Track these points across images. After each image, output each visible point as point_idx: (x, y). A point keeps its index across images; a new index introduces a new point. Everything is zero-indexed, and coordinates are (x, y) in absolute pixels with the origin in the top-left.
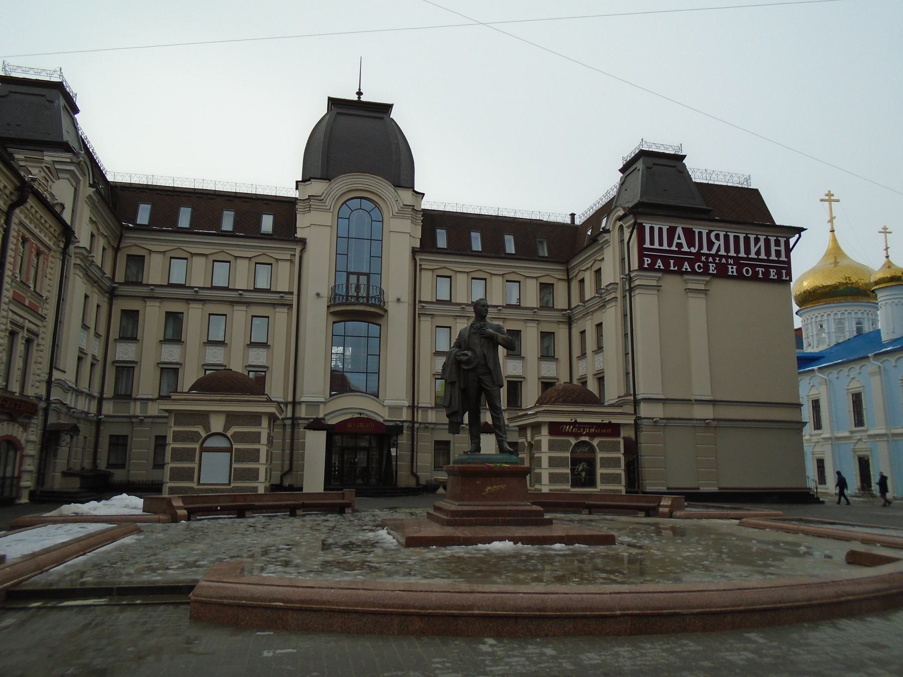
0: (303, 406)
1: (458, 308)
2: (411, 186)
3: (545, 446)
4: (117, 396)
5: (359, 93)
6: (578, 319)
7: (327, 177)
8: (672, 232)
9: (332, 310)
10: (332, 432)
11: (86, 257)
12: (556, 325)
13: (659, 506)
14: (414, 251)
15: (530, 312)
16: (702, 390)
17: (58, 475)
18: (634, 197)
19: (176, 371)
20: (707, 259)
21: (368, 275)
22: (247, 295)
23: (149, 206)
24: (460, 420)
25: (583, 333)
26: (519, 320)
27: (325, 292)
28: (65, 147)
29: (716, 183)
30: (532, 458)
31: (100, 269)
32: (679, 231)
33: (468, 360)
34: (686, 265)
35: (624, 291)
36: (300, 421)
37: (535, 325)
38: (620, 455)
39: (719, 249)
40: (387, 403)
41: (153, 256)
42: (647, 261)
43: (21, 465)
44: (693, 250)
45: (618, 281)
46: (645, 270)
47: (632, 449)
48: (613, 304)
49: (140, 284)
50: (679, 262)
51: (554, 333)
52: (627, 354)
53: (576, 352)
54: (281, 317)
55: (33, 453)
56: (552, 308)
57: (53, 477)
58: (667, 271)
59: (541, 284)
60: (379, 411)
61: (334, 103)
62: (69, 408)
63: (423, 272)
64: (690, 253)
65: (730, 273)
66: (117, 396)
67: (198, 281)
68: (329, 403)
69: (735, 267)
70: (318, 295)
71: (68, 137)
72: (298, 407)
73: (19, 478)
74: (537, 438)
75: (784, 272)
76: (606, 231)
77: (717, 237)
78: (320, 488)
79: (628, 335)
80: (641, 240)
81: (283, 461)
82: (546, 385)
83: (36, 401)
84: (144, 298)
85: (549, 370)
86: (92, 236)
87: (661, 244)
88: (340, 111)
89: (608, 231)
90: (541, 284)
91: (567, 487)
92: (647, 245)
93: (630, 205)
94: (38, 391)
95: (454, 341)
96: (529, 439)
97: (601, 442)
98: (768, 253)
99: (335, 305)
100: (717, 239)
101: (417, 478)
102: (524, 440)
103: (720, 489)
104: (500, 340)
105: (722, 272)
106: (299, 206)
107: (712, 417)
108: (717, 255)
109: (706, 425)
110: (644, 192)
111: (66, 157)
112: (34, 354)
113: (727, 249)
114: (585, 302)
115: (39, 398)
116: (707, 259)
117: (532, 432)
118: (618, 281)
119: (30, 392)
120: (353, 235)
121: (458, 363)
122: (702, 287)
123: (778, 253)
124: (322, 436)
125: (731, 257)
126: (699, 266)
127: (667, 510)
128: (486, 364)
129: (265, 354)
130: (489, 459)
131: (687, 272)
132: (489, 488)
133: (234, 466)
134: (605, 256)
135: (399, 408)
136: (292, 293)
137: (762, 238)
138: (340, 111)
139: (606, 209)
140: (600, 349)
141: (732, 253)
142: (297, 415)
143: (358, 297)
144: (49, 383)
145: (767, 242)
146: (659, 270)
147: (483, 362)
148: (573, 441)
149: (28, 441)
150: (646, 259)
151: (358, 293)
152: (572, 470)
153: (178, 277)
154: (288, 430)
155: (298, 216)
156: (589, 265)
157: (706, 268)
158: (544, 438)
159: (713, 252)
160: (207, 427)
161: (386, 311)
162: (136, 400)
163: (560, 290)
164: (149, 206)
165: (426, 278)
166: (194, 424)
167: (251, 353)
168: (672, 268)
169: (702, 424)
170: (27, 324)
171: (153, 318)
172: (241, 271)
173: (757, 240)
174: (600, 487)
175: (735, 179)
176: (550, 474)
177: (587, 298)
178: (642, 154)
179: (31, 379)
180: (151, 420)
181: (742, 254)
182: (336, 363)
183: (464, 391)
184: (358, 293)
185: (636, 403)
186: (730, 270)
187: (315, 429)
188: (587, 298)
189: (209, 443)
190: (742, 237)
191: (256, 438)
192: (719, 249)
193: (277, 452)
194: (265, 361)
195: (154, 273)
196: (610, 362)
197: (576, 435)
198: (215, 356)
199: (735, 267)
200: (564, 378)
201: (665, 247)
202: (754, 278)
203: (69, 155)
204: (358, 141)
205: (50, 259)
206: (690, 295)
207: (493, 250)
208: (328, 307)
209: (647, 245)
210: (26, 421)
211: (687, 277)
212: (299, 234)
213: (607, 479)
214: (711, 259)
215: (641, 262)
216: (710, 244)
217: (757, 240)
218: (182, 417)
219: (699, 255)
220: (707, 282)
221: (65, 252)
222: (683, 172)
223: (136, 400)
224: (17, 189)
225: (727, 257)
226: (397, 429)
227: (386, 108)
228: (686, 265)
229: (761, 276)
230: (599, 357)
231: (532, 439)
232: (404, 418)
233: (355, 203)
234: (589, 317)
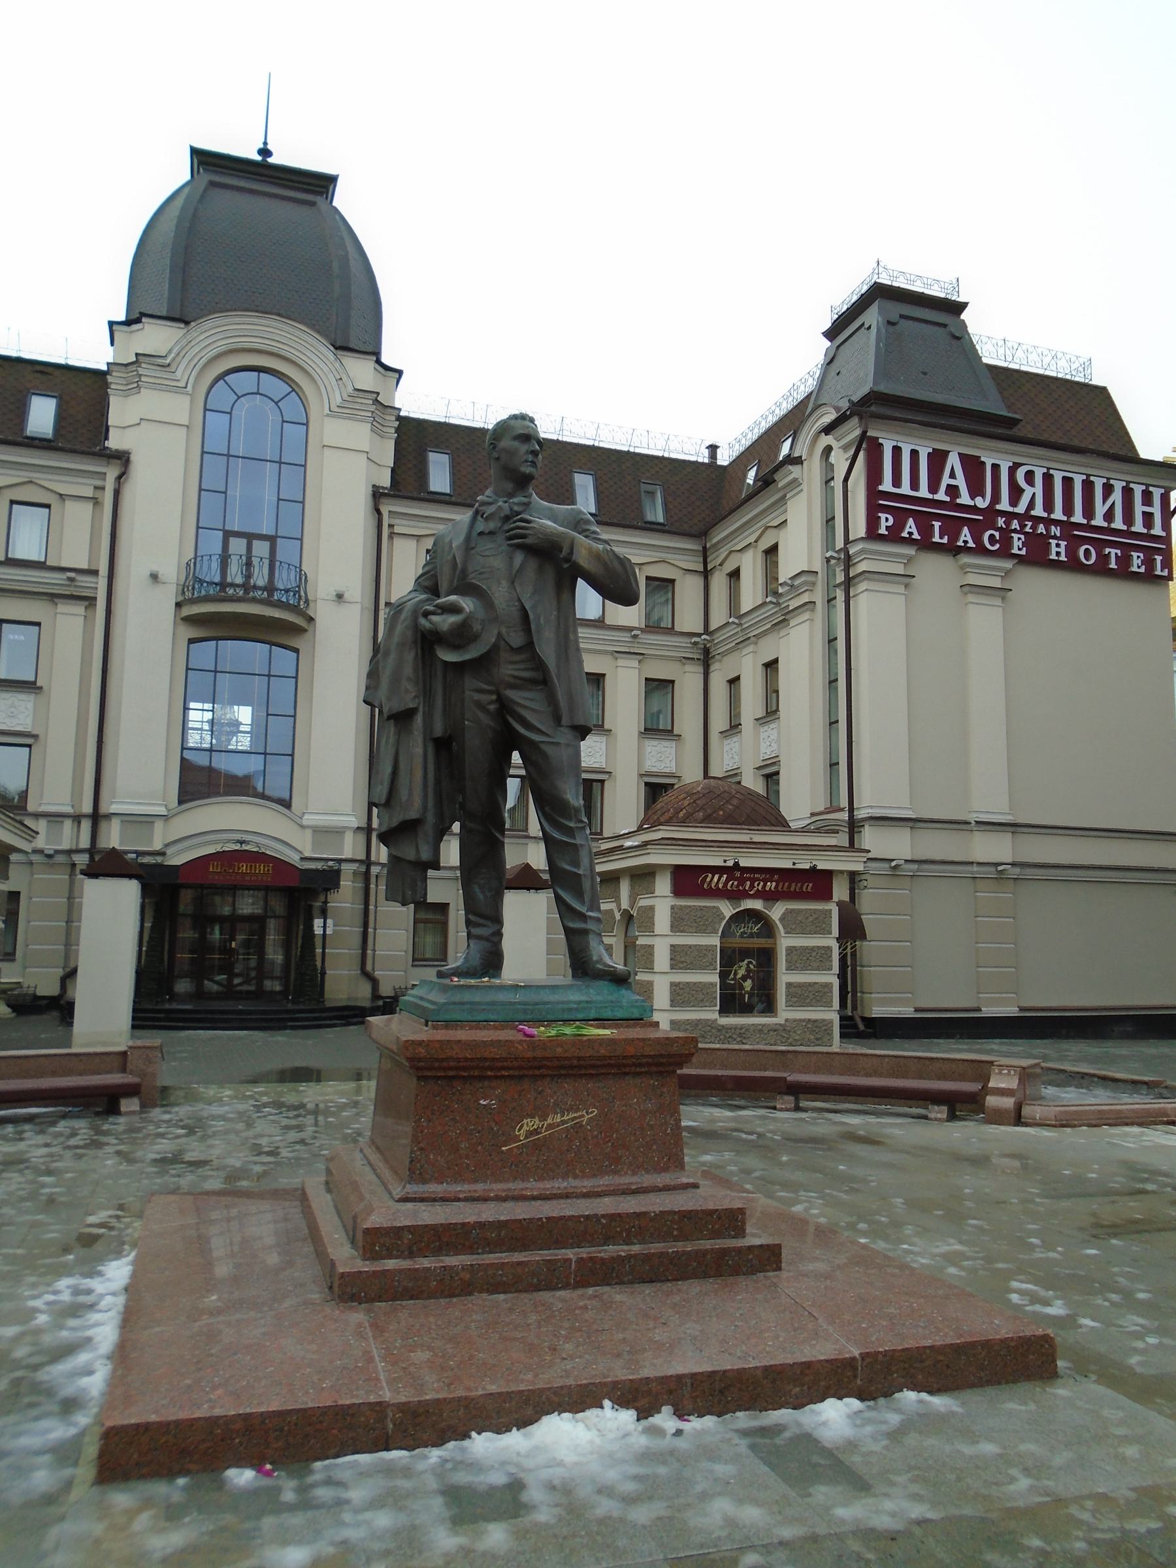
0: (115, 824)
2: (376, 354)
3: (662, 920)
7: (180, 316)
8: (938, 459)
9: (187, 611)
12: (677, 665)
13: (986, 1091)
14: (377, 495)
15: (625, 637)
16: (991, 803)
18: (862, 378)
21: (272, 539)
24: (425, 855)
25: (734, 681)
26: (606, 652)
27: (172, 572)
29: (1024, 368)
30: (630, 946)
32: (953, 461)
33: (464, 626)
34: (965, 535)
35: (830, 586)
37: (635, 664)
38: (831, 942)
40: (308, 819)
42: (886, 521)
44: (981, 503)
45: (818, 566)
46: (881, 538)
47: (852, 929)
48: (806, 616)
50: (952, 527)
51: (673, 682)
52: (833, 723)
53: (719, 721)
54: (68, 628)
56: (670, 631)
58: (925, 544)
60: (289, 838)
61: (205, 160)
63: (397, 542)
64: (974, 509)
65: (1053, 556)
69: (1063, 543)
70: (154, 577)
72: (103, 826)
74: (643, 902)
75: (1159, 558)
76: (792, 460)
79: (839, 683)
82: (655, 790)
85: (661, 758)
87: (915, 485)
88: (217, 178)
89: (798, 461)
92: (887, 486)
93: (855, 399)
96: (625, 904)
98: (1128, 518)
99: (193, 601)
100: (1028, 480)
101: (374, 982)
102: (613, 906)
103: (1022, 1009)
104: (582, 558)
105: (1037, 556)
107: (1010, 860)
108: (1027, 516)
109: (998, 873)
110: (882, 370)
113: (1049, 506)
114: (740, 617)
117: (632, 887)
120: (239, 449)
121: (427, 642)
122: (996, 582)
123: (1148, 518)
124: (128, 892)
125: (1057, 522)
126: (992, 537)
127: (1008, 1103)
128: (529, 646)
129: (30, 705)
130: (533, 1008)
131: (966, 549)
132: (529, 1124)
134: (790, 516)
135: (337, 832)
137: (1118, 486)
138: (217, 178)
139: (792, 422)
140: (771, 713)
141: (1058, 514)
143: (246, 586)
145: (1128, 492)
146: (909, 541)
147: (517, 640)
148: (727, 909)
150: (883, 516)
151: (248, 576)
152: (723, 975)
155: (113, 400)
156: (752, 539)
157: (1006, 541)
158: (662, 900)
161: (311, 620)
163: (688, 591)
173: (1108, 489)
175: (1062, 363)
176: (672, 984)
177: (744, 609)
178: (879, 293)
181: (1078, 517)
183: (444, 747)
185: (854, 826)
186: (1054, 549)
188: (744, 609)
190: (1078, 480)
194: (29, 721)
197: (734, 896)
199: (1063, 543)
200: (692, 774)
201: (923, 492)
202: (1101, 569)
206: (971, 598)
208: (178, 605)
209: (887, 486)
211: (965, 559)
212: (115, 442)
213: (802, 995)
214: (1015, 524)
215: (872, 522)
216: (1016, 493)
217: (1108, 489)
219: (991, 513)
220: (1008, 573)
222: (960, 339)
225: (1049, 522)
226: (328, 878)
227: (323, 184)
228: (965, 535)
229: (1113, 565)
230: (770, 732)
231: (632, 904)
232: (347, 853)
234: (751, 648)
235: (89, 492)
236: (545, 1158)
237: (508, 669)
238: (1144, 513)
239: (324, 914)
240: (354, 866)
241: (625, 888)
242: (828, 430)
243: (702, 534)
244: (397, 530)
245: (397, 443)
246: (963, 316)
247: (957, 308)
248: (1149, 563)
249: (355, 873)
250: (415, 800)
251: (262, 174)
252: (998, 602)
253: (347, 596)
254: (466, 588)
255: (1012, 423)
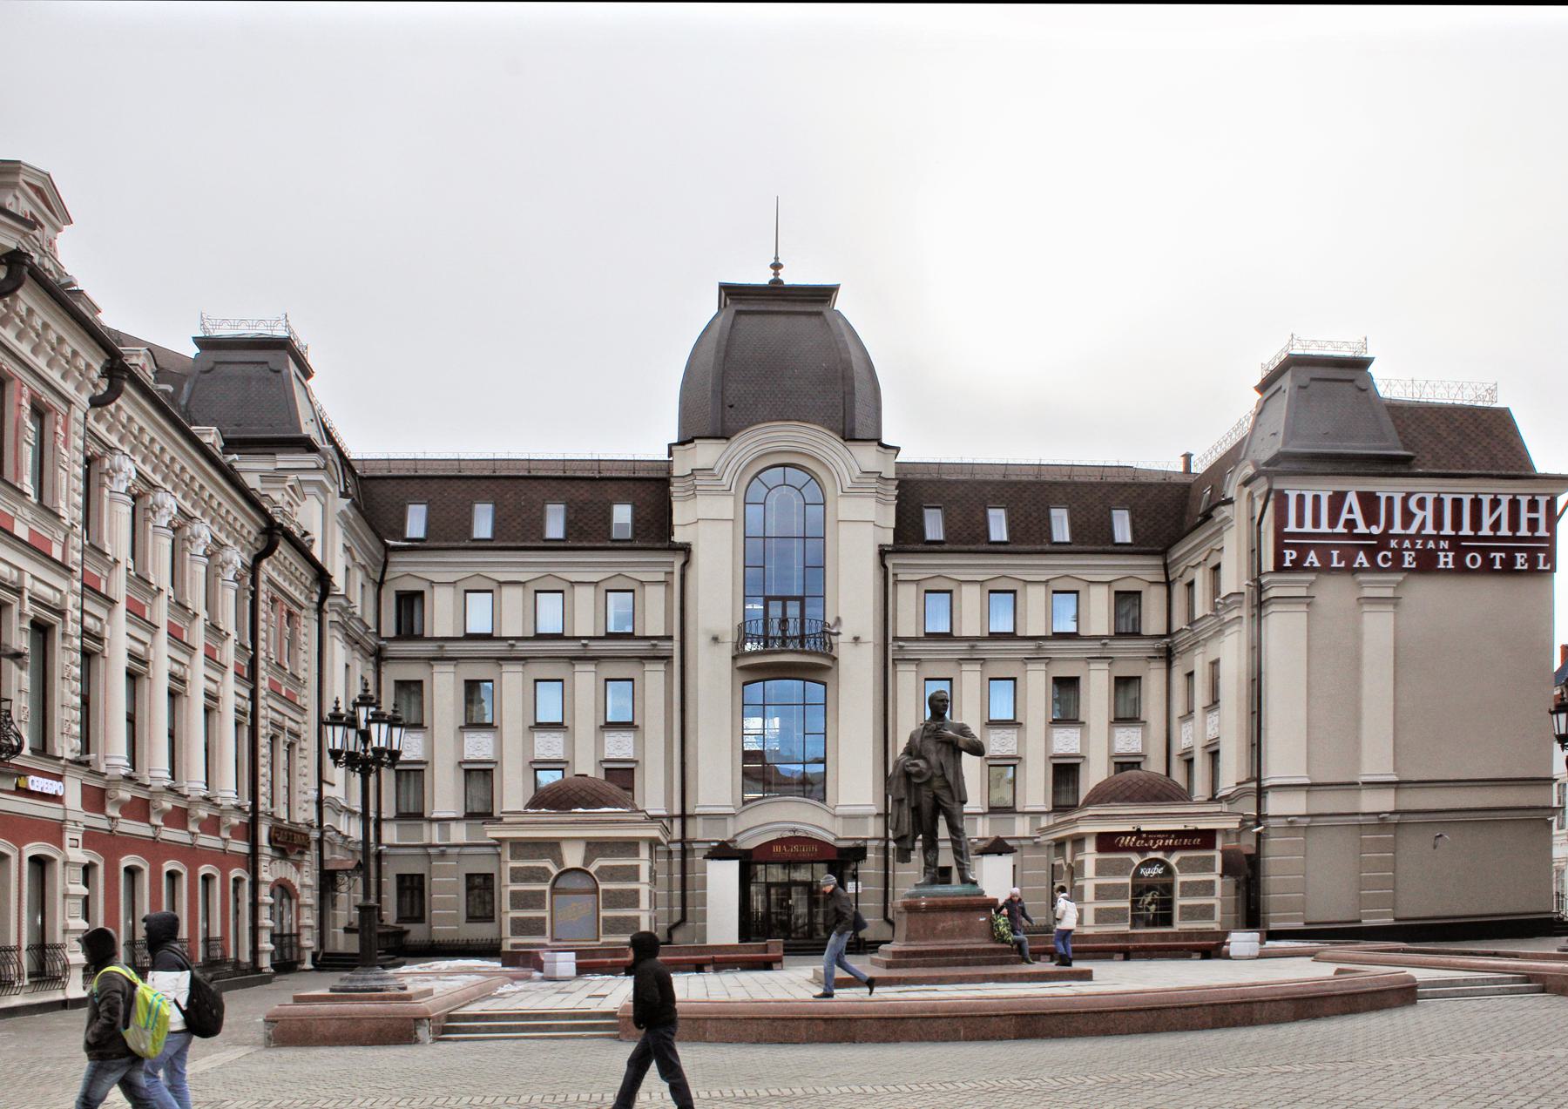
1: (964, 646)
4: (401, 816)
5: (776, 266)
6: (1183, 653)
8: (1337, 500)
10: (749, 862)
11: (345, 609)
14: (883, 553)
15: (1097, 645)
17: (340, 931)
19: (487, 773)
20: (1400, 544)
22: (594, 645)
23: (423, 508)
25: (1190, 675)
28: (307, 445)
31: (361, 620)
32: (1352, 499)
36: (695, 846)
37: (1105, 666)
39: (1423, 525)
40: (839, 811)
41: (438, 590)
42: (1290, 556)
43: (298, 918)
44: (1375, 530)
48: (1235, 628)
49: (421, 638)
50: (1348, 555)
54: (654, 678)
55: (310, 901)
56: (1136, 634)
57: (335, 934)
58: (1326, 569)
59: (1117, 593)
62: (346, 837)
63: (901, 587)
64: (1370, 536)
65: (1441, 566)
66: (401, 816)
67: (512, 627)
68: (742, 817)
69: (1451, 554)
71: (309, 430)
72: (690, 822)
73: (298, 935)
75: (1541, 556)
77: (1421, 504)
78: (733, 939)
80: (1281, 520)
81: (670, 906)
83: (305, 829)
84: (431, 660)
85: (1128, 741)
86: (347, 569)
87: (1316, 523)
90: (1117, 593)
91: (1125, 928)
92: (1292, 527)
94: (306, 815)
95: (901, 741)
97: (1183, 859)
100: (1418, 505)
105: (1427, 564)
106: (676, 489)
107: (1392, 809)
108: (1418, 535)
109: (1381, 821)
111: (310, 460)
112: (299, 763)
113: (1439, 524)
115: (310, 826)
116: (1400, 544)
118: (1244, 589)
119: (299, 817)
120: (772, 532)
123: (1533, 524)
125: (1445, 538)
131: (1362, 570)
133: (603, 913)
136: (670, 638)
137: (1505, 500)
139: (1232, 458)
140: (1215, 703)
142: (690, 835)
144: (320, 802)
146: (1312, 569)
149: (303, 886)
150: (1287, 552)
151: (784, 631)
152: (1134, 903)
153: (479, 623)
154: (677, 860)
155: (676, 507)
156: (1201, 559)
157: (1398, 556)
158: (1090, 856)
159: (1413, 530)
160: (559, 861)
161: (835, 659)
162: (432, 820)
163: (1153, 602)
164: (423, 508)
165: (906, 598)
166: (541, 857)
167: (607, 740)
168: (1335, 564)
169: (1374, 820)
170: (288, 723)
171: (444, 688)
172: (579, 599)
173: (1495, 503)
174: (1179, 925)
178: (1294, 363)
179: (298, 798)
180: (457, 850)
181: (1466, 530)
182: (753, 745)
183: (916, 811)
184: (784, 631)
185: (1261, 792)
187: (720, 858)
189: (561, 884)
191: (632, 874)
192: (1423, 525)
193: (663, 893)
195: (441, 618)
196: (1228, 726)
197: (1142, 850)
198: (549, 746)
199: (1451, 554)
201: (1324, 528)
202: (1488, 568)
203: (314, 456)
204: (778, 357)
205: (303, 621)
207: (1030, 537)
208: (734, 658)
209: (1292, 527)
210: (298, 858)
211: (1361, 577)
212: (679, 537)
213: (1189, 913)
214: (1407, 544)
215: (1279, 557)
216: (1408, 517)
218: (521, 847)
219: (1385, 537)
221: (320, 610)
222: (1366, 389)
223: (432, 820)
224: (263, 532)
225: (1437, 538)
227: (825, 294)
228: (1362, 558)
229: (1498, 566)
230: (1212, 718)
233: (775, 475)
235: (661, 577)
236: (950, 933)
237: (937, 783)
238: (1529, 520)
239: (855, 878)
240: (876, 843)
241: (1068, 848)
242: (1246, 483)
243: (1164, 553)
244: (900, 577)
245: (898, 506)
246: (1370, 370)
247: (1361, 364)
248: (1532, 561)
249: (877, 848)
250: (906, 828)
251: (776, 293)
252: (1391, 608)
253: (863, 639)
254: (920, 756)
255: (1406, 460)
